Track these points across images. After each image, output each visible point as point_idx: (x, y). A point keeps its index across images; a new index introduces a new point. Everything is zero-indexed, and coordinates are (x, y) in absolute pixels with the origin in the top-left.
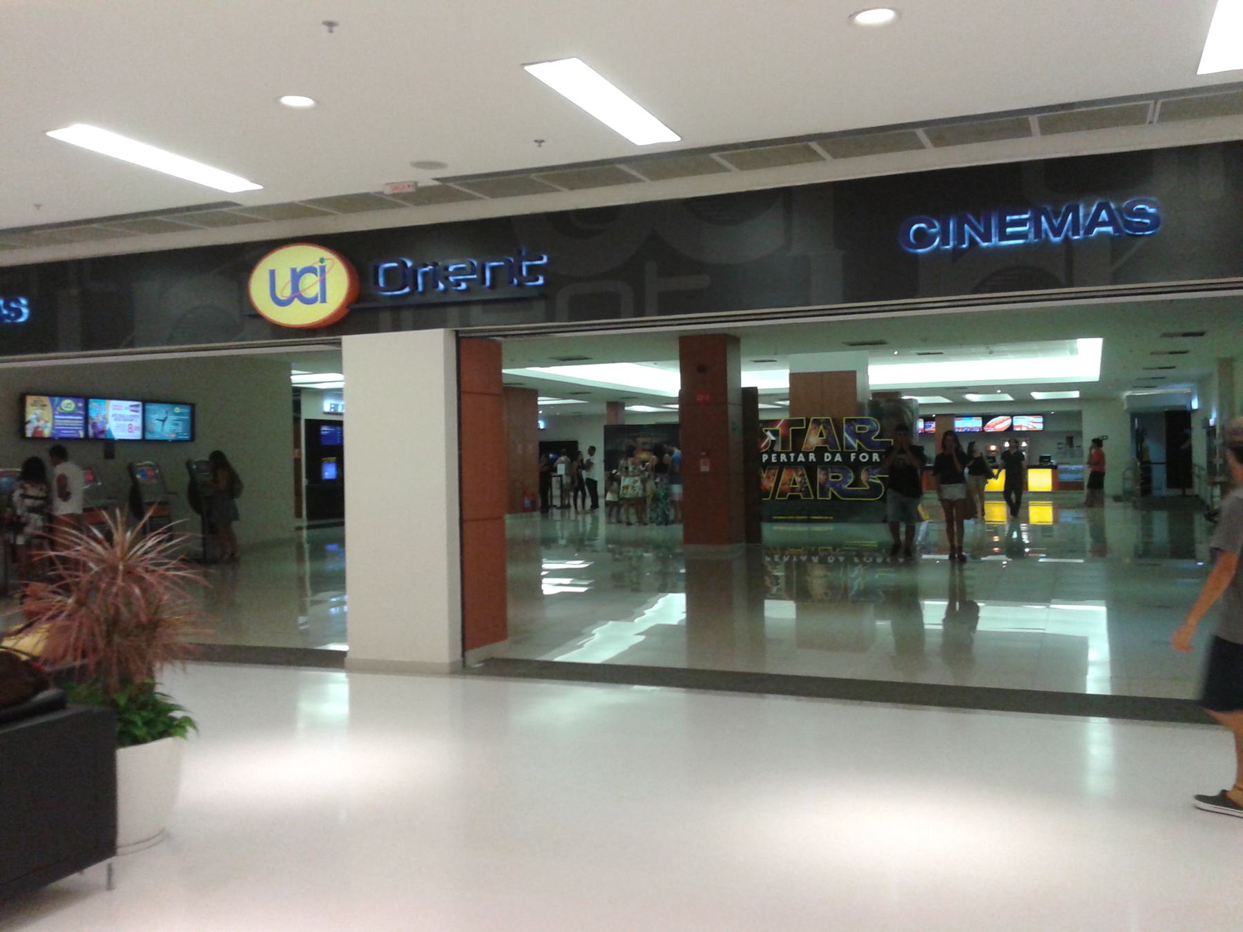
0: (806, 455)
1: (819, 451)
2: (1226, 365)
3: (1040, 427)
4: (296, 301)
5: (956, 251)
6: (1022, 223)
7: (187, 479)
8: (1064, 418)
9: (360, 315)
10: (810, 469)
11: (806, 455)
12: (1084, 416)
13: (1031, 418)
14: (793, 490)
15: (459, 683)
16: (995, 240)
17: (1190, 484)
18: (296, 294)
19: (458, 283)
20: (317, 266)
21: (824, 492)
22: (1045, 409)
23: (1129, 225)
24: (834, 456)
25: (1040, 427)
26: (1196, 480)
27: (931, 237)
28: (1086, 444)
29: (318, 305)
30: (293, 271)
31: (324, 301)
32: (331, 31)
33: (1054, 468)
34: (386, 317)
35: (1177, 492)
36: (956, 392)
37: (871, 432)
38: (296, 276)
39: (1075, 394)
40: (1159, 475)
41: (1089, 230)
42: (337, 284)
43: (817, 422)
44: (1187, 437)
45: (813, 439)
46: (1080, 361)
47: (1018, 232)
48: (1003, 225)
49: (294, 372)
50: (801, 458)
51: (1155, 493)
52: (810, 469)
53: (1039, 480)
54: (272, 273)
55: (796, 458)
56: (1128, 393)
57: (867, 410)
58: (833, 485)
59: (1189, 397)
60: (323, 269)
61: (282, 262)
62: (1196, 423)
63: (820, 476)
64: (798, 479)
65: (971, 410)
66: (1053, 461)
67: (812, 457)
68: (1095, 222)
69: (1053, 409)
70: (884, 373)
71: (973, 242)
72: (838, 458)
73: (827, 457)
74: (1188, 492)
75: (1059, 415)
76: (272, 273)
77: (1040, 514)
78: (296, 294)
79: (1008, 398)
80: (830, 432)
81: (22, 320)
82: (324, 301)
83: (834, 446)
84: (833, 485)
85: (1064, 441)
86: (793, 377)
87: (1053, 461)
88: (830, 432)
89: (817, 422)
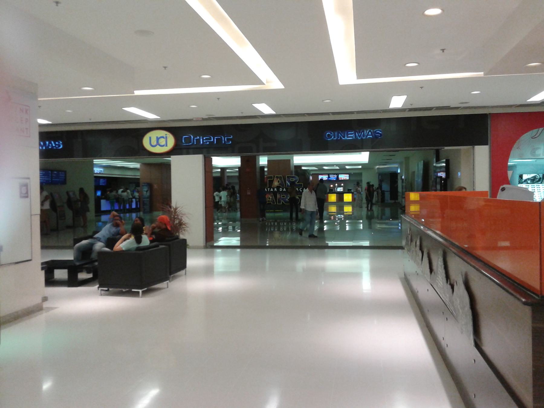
0: (274, 189)
1: (278, 187)
2: (407, 159)
3: (348, 178)
4: (158, 146)
5: (337, 140)
6: (352, 134)
7: (67, 197)
8: (356, 174)
9: (176, 150)
10: (275, 194)
11: (274, 189)
12: (363, 174)
13: (345, 175)
14: (269, 201)
15: (205, 250)
16: (346, 138)
17: (397, 199)
18: (158, 144)
19: (206, 142)
20: (165, 136)
21: (279, 202)
22: (348, 172)
23: (375, 136)
24: (283, 189)
25: (348, 178)
26: (399, 197)
27: (332, 136)
28: (364, 185)
29: (165, 147)
30: (157, 137)
31: (166, 146)
32: (57, 5)
33: (352, 193)
34: (185, 151)
35: (393, 201)
36: (320, 167)
37: (296, 181)
38: (158, 139)
39: (360, 167)
40: (387, 196)
41: (367, 136)
42: (171, 141)
43: (277, 177)
44: (397, 182)
45: (276, 183)
46: (362, 157)
47: (350, 136)
48: (348, 134)
49: (237, 174)
50: (272, 190)
51: (386, 201)
52: (275, 194)
53: (348, 197)
54: (150, 138)
55: (270, 190)
56: (377, 167)
57: (294, 173)
58: (283, 199)
59: (397, 168)
60: (166, 137)
61: (154, 135)
62: (399, 177)
63: (278, 196)
64: (271, 197)
65: (324, 172)
66: (352, 191)
67: (275, 189)
68: (368, 135)
69: (352, 172)
70: (299, 160)
71: (341, 138)
72: (284, 190)
73: (281, 190)
74: (397, 201)
75: (355, 174)
76: (150, 138)
77: (348, 209)
78: (158, 144)
79: (338, 168)
80: (282, 181)
81: (61, 147)
82: (166, 146)
83: (283, 185)
84: (283, 199)
85: (356, 183)
86: (268, 161)
87: (352, 191)
88: (282, 181)
89: (277, 177)
